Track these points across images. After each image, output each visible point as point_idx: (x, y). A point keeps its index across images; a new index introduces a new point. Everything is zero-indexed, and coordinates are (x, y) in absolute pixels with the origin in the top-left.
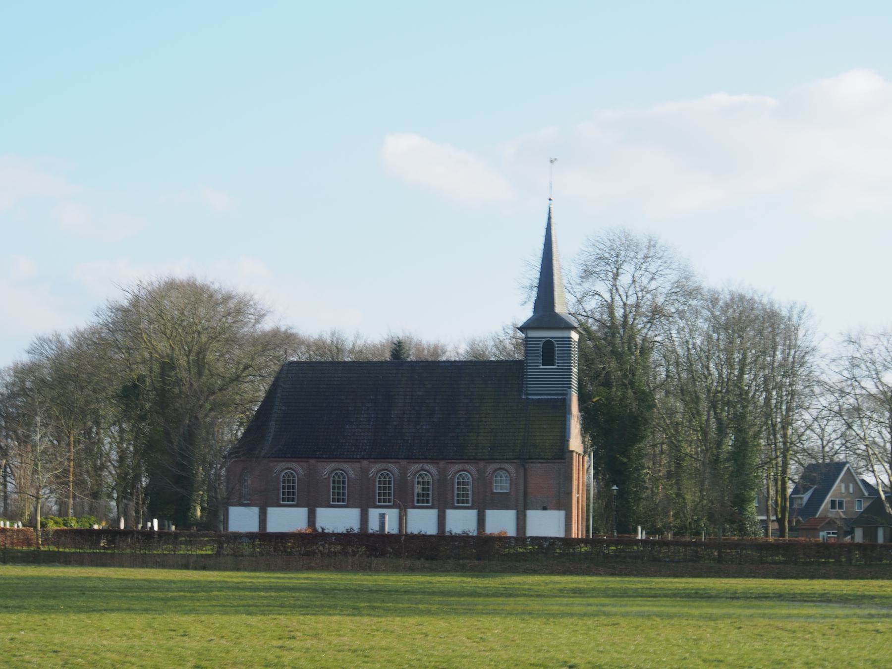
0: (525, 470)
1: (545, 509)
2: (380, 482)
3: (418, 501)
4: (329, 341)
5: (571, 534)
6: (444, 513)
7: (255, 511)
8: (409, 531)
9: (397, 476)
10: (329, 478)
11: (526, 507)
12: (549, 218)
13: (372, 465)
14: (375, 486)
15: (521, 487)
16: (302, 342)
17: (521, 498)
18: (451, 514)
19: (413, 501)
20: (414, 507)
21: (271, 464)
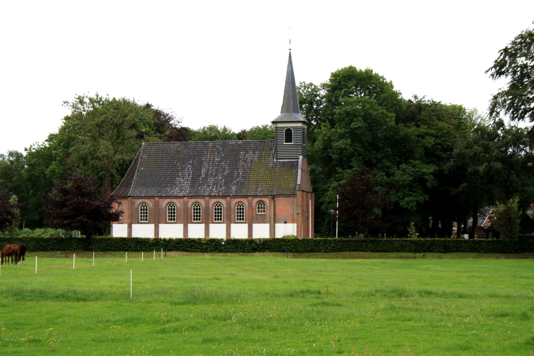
0: (274, 201)
1: (285, 223)
2: (141, 210)
3: (141, 220)
4: (63, 125)
5: (308, 236)
6: (230, 225)
7: (152, 226)
8: (160, 237)
9: (204, 206)
10: (166, 207)
11: (275, 222)
12: (290, 54)
13: (189, 200)
14: (191, 212)
15: (272, 211)
16: (196, 133)
17: (272, 216)
18: (255, 226)
19: (213, 219)
20: (139, 223)
21: (134, 200)
